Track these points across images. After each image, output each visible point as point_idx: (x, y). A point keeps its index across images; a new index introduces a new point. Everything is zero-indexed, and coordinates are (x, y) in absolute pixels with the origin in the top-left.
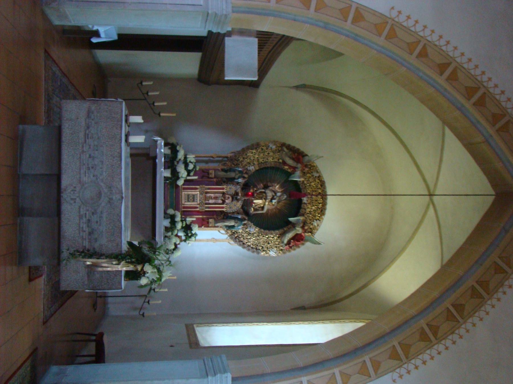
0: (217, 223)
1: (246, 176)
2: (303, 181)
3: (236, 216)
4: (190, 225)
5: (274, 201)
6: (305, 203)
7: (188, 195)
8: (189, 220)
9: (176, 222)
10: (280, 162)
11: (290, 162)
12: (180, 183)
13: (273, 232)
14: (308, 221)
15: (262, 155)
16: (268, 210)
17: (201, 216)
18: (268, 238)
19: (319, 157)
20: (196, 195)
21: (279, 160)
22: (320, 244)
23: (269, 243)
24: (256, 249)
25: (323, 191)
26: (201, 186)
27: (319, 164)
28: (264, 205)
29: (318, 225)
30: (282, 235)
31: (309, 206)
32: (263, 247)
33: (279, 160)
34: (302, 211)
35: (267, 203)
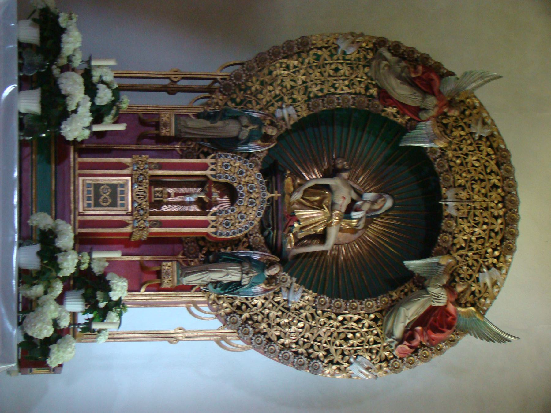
1: (272, 132)
3: (243, 252)
4: (105, 274)
5: (355, 215)
6: (450, 217)
7: (97, 186)
8: (101, 257)
9: (59, 250)
10: (371, 96)
11: (402, 92)
12: (76, 129)
13: (356, 304)
14: (464, 271)
15: (316, 74)
16: (337, 244)
17: (137, 258)
18: (342, 322)
19: (487, 79)
20: (122, 186)
21: (367, 88)
22: (504, 340)
23: (346, 339)
24: (309, 356)
25: (504, 179)
26: (137, 158)
27: (485, 96)
28: (328, 225)
29: (494, 284)
30: (391, 309)
31: (465, 225)
32: (328, 351)
33: (367, 88)
34: (443, 239)
35: (335, 220)
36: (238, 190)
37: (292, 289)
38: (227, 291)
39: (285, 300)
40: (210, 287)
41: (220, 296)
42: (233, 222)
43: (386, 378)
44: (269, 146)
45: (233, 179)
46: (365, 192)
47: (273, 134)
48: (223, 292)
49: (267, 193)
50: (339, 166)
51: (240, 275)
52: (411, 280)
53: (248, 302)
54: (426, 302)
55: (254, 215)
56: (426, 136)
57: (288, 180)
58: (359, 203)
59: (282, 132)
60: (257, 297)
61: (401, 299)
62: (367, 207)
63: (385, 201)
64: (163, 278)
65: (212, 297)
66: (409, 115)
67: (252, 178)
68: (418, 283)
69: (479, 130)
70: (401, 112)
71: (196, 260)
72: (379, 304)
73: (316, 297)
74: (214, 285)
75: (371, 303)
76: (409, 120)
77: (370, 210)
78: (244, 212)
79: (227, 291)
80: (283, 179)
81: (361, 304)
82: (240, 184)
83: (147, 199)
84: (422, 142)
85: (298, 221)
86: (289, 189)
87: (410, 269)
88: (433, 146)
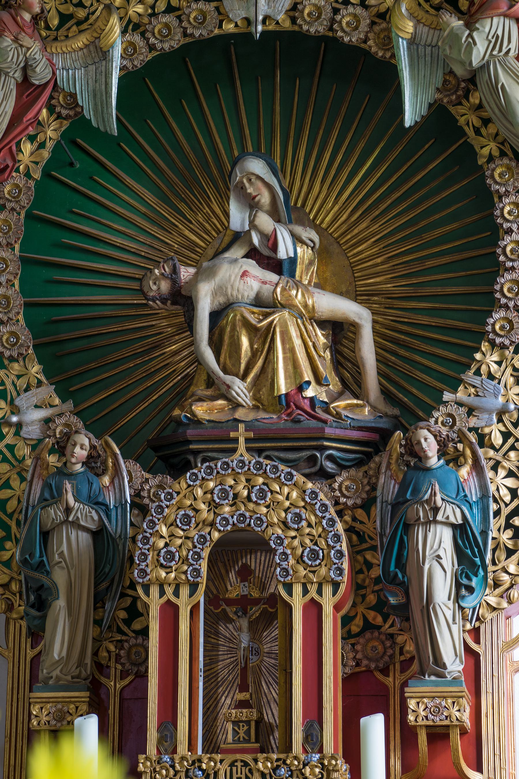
0: (438, 661)
2: (130, 26)
5: (285, 248)
36: (229, 528)
37: (472, 401)
38: (478, 560)
39: (500, 420)
40: (470, 602)
41: (490, 582)
42: (308, 541)
44: (115, 455)
45: (203, 540)
46: (227, 228)
47: (86, 442)
48: (481, 572)
49: (236, 456)
50: (165, 286)
51: (439, 527)
52: (452, 110)
53: (505, 511)
54: (509, 70)
55: (291, 490)
56: (92, 68)
57: (200, 410)
58: (256, 240)
59: (80, 425)
60: (492, 488)
61: (497, 134)
62: (265, 221)
63: (251, 176)
64: (447, 722)
65: (492, 600)
66: (39, 111)
67: (200, 492)
68: (460, 93)
70: (31, 131)
71: (400, 639)
72: (510, 189)
73: (493, 344)
74: (463, 592)
75: (507, 209)
76: (51, 109)
77: (274, 214)
78: (283, 515)
79: (478, 560)
80: (196, 422)
81: (509, 231)
82: (212, 524)
83: (248, 758)
84: (108, 75)
85: (300, 389)
86: (221, 410)
87: (424, 112)
88: (117, 52)
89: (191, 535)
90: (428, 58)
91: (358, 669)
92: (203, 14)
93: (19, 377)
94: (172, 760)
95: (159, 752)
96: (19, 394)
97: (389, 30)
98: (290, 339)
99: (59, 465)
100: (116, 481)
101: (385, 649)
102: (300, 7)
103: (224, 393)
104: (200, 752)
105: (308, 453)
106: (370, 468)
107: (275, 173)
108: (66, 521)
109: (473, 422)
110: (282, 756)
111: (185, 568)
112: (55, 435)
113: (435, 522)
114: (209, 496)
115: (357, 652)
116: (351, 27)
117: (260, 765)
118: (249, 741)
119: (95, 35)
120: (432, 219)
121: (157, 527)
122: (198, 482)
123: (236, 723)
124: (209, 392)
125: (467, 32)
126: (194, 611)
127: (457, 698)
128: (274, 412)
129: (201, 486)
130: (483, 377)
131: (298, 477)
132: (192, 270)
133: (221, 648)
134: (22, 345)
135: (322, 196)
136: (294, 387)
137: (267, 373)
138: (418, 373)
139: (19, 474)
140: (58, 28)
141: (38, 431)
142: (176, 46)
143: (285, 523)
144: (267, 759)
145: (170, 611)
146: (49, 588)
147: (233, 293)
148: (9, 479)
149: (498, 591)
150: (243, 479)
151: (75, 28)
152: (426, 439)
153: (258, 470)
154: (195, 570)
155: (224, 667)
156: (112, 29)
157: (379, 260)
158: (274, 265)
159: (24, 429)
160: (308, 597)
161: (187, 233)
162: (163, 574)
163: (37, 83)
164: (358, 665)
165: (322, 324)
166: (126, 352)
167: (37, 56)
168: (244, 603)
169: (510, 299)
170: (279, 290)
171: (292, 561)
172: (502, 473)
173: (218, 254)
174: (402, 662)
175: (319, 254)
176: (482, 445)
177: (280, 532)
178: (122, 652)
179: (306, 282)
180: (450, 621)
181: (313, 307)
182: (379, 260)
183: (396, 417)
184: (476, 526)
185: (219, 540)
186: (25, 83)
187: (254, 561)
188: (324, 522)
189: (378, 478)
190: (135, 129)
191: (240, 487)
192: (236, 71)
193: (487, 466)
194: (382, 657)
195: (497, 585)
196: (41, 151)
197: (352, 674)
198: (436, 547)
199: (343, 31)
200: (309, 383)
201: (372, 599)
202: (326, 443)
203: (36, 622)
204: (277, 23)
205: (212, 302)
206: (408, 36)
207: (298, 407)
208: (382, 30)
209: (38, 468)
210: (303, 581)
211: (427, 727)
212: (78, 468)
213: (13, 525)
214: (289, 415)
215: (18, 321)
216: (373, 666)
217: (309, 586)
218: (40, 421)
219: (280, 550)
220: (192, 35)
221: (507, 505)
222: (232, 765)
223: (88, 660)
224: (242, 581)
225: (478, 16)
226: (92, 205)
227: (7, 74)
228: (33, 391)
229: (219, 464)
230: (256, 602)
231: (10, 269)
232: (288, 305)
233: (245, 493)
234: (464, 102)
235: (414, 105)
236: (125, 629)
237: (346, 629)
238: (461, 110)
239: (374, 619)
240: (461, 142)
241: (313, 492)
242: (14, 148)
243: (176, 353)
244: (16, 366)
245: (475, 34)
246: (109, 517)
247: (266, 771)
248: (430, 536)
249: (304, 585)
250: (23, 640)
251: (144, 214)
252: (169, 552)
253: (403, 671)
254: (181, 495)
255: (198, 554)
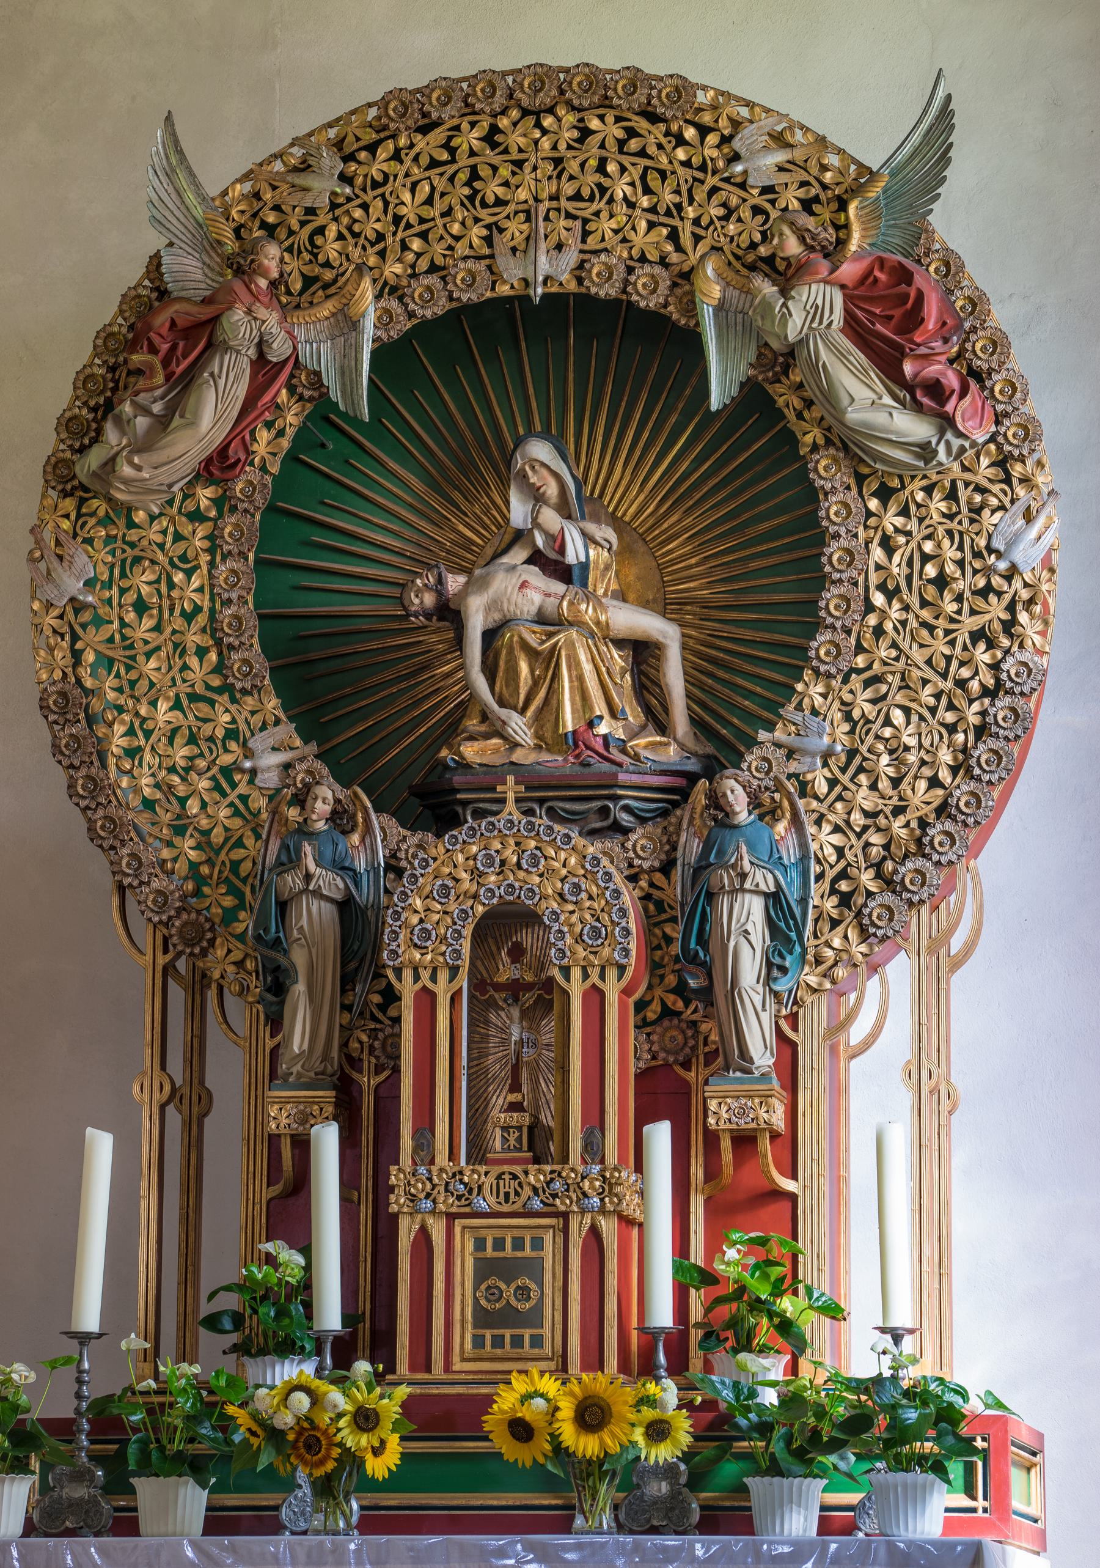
2: (387, 290)
5: (575, 551)
11: (212, 414)
14: (743, 229)
36: (495, 901)
38: (793, 935)
39: (825, 764)
40: (783, 985)
41: (810, 957)
42: (588, 917)
43: (1051, 468)
44: (365, 808)
47: (329, 795)
48: (798, 949)
50: (429, 599)
51: (747, 896)
52: (770, 388)
53: (830, 874)
57: (470, 751)
58: (540, 541)
59: (325, 771)
60: (814, 847)
61: (822, 418)
62: (550, 518)
63: (533, 463)
64: (753, 1126)
65: (813, 980)
67: (460, 858)
68: (778, 369)
69: (323, 186)
70: (268, 416)
71: (704, 1027)
72: (837, 485)
73: (816, 672)
74: (775, 973)
75: (834, 509)
76: (292, 390)
77: (564, 510)
78: (559, 885)
79: (793, 935)
80: (464, 766)
81: (836, 536)
82: (475, 897)
83: (518, 1169)
84: (358, 349)
85: (591, 725)
86: (496, 751)
87: (734, 392)
89: (450, 909)
90: (740, 328)
91: (654, 1063)
92: (472, 274)
93: (253, 713)
94: (429, 1171)
95: (414, 1163)
96: (253, 734)
97: (692, 293)
98: (578, 664)
99: (301, 820)
100: (367, 840)
101: (686, 1039)
102: (587, 266)
103: (498, 731)
104: (463, 1163)
105: (596, 804)
106: (670, 823)
107: (565, 459)
108: (306, 890)
109: (793, 767)
110: (557, 1167)
111: (444, 948)
112: (295, 784)
113: (743, 890)
114: (471, 862)
115: (652, 1043)
116: (649, 292)
117: (531, 1178)
118: (520, 1150)
119: (344, 301)
120: (757, 510)
121: (410, 901)
122: (458, 847)
123: (505, 1129)
124: (483, 728)
125: (782, 300)
126: (455, 999)
127: (765, 1098)
128: (559, 753)
129: (462, 851)
130: (807, 712)
131: (578, 840)
132: (462, 579)
133: (492, 1039)
134: (256, 675)
135: (624, 482)
136: (582, 723)
137: (550, 707)
138: (740, 699)
139: (254, 830)
140: (300, 294)
141: (276, 779)
142: (440, 313)
143: (561, 895)
144: (539, 1171)
145: (426, 999)
146: (286, 970)
147: (510, 609)
148: (242, 836)
149: (820, 969)
150: (512, 841)
151: (320, 293)
152: (732, 791)
153: (530, 831)
154: (455, 951)
155: (496, 1062)
156: (363, 295)
157: (693, 561)
158: (562, 572)
159: (259, 776)
160: (589, 983)
161: (461, 528)
162: (418, 956)
163: (274, 360)
164: (654, 1058)
165: (619, 643)
166: (388, 675)
167: (273, 330)
168: (515, 989)
169: (837, 618)
170: (565, 604)
171: (569, 940)
172: (827, 828)
173: (497, 555)
174: (706, 1054)
175: (617, 554)
176: (803, 794)
177: (555, 905)
178: (377, 1044)
179: (601, 592)
180: (759, 1008)
181: (607, 624)
182: (693, 561)
183: (708, 757)
184: (793, 894)
185: (485, 916)
186: (261, 361)
187: (527, 938)
188: (608, 894)
189: (679, 836)
190: (400, 402)
191: (508, 853)
192: (521, 330)
193: (808, 820)
194: (682, 1049)
195: (818, 961)
196: (280, 439)
197: (647, 1069)
198: (743, 920)
199: (639, 294)
200: (601, 718)
201: (671, 980)
202: (620, 792)
203: (274, 1008)
204: (561, 284)
205: (486, 619)
206: (716, 302)
207: (588, 748)
208: (685, 294)
209: (275, 824)
210: (582, 963)
211: (731, 1131)
212: (321, 825)
213: (248, 891)
214: (577, 756)
215: (252, 645)
216: (671, 1059)
217: (589, 970)
218: (278, 766)
219: (556, 927)
220: (459, 299)
221: (832, 867)
222: (499, 1177)
223: (335, 1054)
224: (513, 962)
225: (794, 281)
226: (349, 496)
227: (238, 352)
228: (270, 729)
229: (483, 825)
230: (529, 987)
231: (242, 583)
232: (576, 623)
233: (515, 859)
234: (783, 379)
235: (722, 385)
236: (380, 1015)
237: (641, 1015)
238: (779, 388)
239: (674, 1004)
240: (778, 428)
241: (594, 858)
242: (248, 437)
243: (448, 675)
244: (249, 700)
245: (790, 304)
246: (357, 884)
247: (538, 1185)
248: (736, 907)
249: (584, 968)
250: (261, 1027)
251: (411, 505)
252: (424, 930)
253: (706, 1065)
254: (438, 862)
255: (459, 932)
